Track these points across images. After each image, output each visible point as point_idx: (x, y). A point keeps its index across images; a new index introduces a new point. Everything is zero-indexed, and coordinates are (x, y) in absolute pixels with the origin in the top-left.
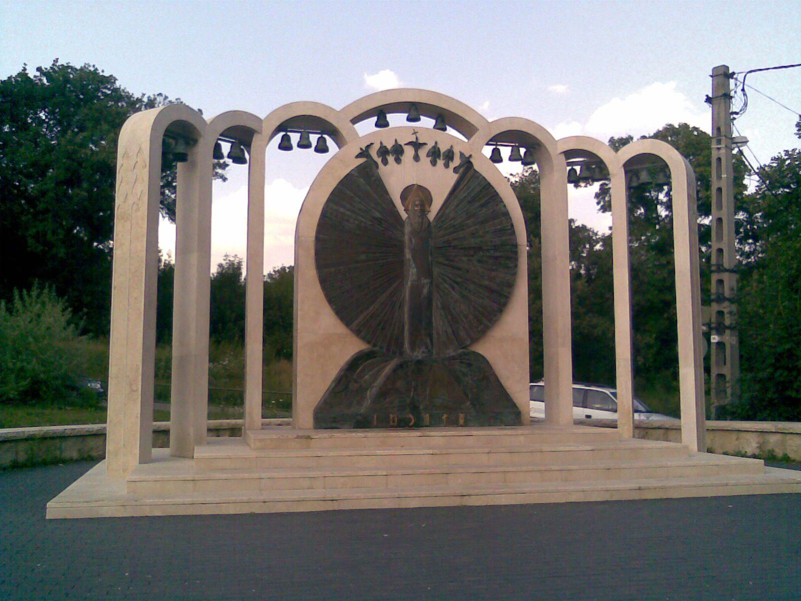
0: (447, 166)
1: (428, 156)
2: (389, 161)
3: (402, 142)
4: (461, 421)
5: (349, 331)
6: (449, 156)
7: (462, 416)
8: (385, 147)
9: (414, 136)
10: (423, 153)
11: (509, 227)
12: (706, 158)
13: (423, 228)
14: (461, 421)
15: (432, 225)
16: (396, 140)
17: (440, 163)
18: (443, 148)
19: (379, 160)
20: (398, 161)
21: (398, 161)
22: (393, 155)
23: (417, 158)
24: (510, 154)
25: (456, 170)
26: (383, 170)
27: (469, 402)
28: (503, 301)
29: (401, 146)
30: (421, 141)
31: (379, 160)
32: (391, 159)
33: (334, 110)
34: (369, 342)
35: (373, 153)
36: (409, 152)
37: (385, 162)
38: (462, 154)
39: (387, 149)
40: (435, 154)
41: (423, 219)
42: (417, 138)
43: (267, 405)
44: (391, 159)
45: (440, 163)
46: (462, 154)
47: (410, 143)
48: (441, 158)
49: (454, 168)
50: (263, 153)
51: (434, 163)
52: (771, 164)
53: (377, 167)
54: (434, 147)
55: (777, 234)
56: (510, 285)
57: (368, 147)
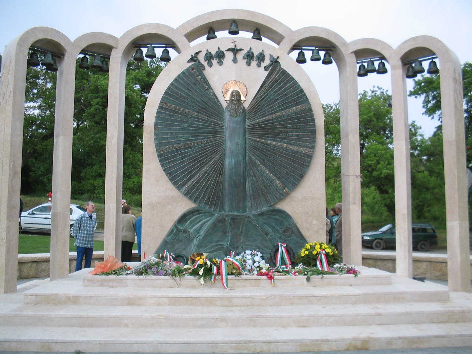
0: (259, 65)
1: (244, 58)
2: (213, 63)
3: (223, 49)
6: (261, 58)
8: (210, 53)
10: (240, 56)
15: (247, 111)
19: (205, 64)
20: (220, 63)
21: (220, 63)
22: (216, 59)
23: (235, 60)
24: (297, 56)
25: (266, 68)
30: (238, 48)
31: (205, 64)
32: (215, 62)
35: (201, 58)
36: (229, 56)
37: (210, 65)
40: (250, 57)
42: (235, 46)
44: (215, 62)
45: (254, 63)
47: (229, 50)
48: (255, 59)
49: (265, 67)
51: (249, 64)
54: (248, 52)
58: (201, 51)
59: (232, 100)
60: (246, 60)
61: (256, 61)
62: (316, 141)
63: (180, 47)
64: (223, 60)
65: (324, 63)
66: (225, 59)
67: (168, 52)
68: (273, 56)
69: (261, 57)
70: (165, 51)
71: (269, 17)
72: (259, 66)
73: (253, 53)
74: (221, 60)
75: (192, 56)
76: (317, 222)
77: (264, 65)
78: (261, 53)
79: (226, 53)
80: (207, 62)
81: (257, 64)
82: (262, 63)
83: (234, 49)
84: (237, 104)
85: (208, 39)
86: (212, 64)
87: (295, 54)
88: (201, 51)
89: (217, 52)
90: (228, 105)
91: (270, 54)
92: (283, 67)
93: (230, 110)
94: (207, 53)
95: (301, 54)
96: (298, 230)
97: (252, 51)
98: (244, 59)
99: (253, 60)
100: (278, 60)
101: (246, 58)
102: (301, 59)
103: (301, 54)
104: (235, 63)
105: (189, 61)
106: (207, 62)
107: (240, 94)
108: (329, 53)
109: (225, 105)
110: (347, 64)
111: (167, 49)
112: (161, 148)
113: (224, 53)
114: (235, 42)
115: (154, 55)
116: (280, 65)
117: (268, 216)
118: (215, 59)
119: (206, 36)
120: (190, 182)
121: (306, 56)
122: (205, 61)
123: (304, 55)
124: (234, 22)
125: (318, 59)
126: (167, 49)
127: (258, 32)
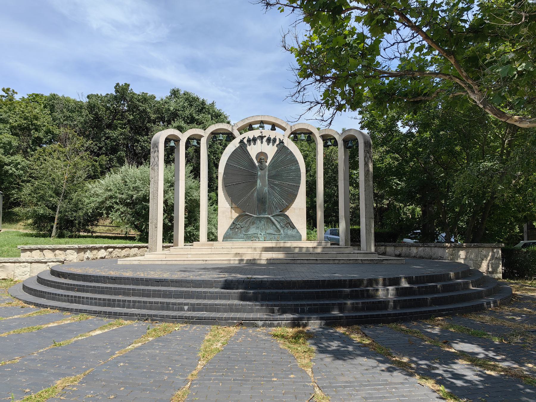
0: (273, 145)
12: (213, 118)
13: (35, 232)
20: (255, 144)
21: (255, 144)
23: (262, 143)
26: (249, 148)
30: (263, 135)
32: (252, 144)
37: (250, 145)
38: (280, 139)
40: (269, 140)
43: (423, 106)
44: (252, 144)
45: (271, 144)
51: (268, 144)
54: (268, 137)
55: (344, 104)
56: (298, 187)
57: (243, 139)
73: (271, 138)
77: (275, 144)
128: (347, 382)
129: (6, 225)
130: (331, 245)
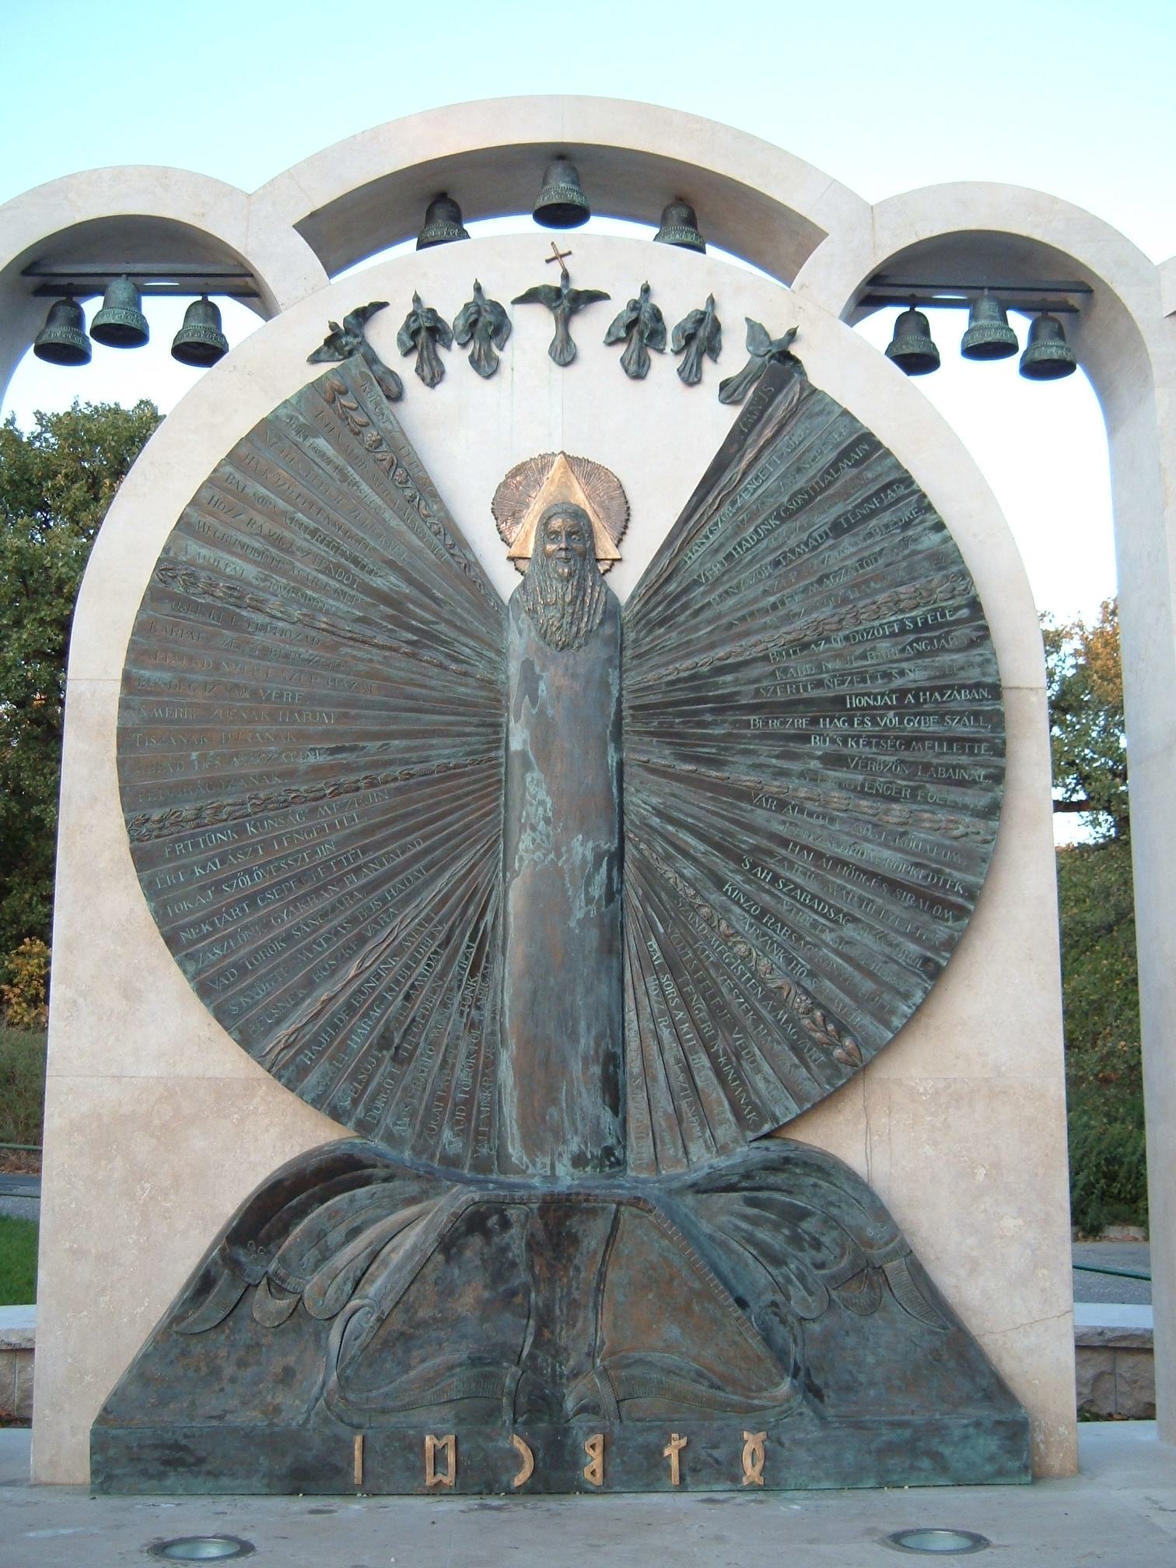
0: (691, 377)
1: (612, 341)
2: (448, 367)
3: (502, 293)
4: (751, 1471)
5: (260, 1072)
7: (752, 1443)
8: (432, 311)
9: (556, 269)
11: (964, 613)
14: (751, 1471)
15: (626, 615)
16: (478, 289)
17: (665, 365)
18: (675, 313)
19: (405, 368)
20: (485, 366)
21: (485, 366)
22: (464, 345)
23: (564, 353)
24: (890, 338)
25: (729, 391)
27: (788, 1380)
28: (941, 931)
29: (496, 307)
30: (579, 285)
31: (405, 368)
32: (455, 359)
33: (232, 191)
34: (337, 1115)
37: (433, 375)
38: (756, 331)
39: (439, 320)
41: (581, 588)
42: (566, 276)
44: (455, 359)
45: (665, 365)
46: (756, 331)
47: (531, 297)
48: (670, 346)
49: (724, 385)
50: (737, 376)
51: (638, 370)
52: (428, 380)
53: (396, 395)
54: (635, 306)
57: (363, 315)
58: (384, 305)
59: (549, 556)
60: (620, 350)
61: (677, 353)
62: (1010, 774)
63: (270, 285)
64: (501, 349)
65: (1035, 369)
66: (508, 345)
67: (214, 314)
68: (767, 328)
69: (702, 333)
70: (201, 310)
71: (739, 135)
72: (693, 379)
73: (657, 315)
74: (490, 346)
75: (333, 326)
76: (1020, 1222)
77: (714, 373)
78: (704, 313)
79: (518, 316)
80: (413, 360)
81: (680, 372)
82: (707, 363)
83: (558, 292)
84: (571, 575)
85: (420, 246)
86: (442, 373)
87: (883, 322)
88: (384, 305)
89: (467, 306)
90: (523, 585)
91: (747, 319)
92: (816, 379)
93: (535, 611)
94: (413, 314)
95: (913, 327)
96: (917, 1271)
97: (657, 300)
98: (611, 344)
99: (661, 351)
100: (795, 350)
101: (618, 341)
102: (913, 347)
103: (913, 327)
104: (566, 364)
105: (318, 352)
106: (414, 359)
107: (590, 524)
108: (1054, 320)
109: (506, 581)
110: (1157, 373)
111: (211, 299)
112: (156, 816)
113: (503, 313)
114: (566, 260)
115: (134, 324)
116: (803, 373)
117: (746, 1193)
118: (455, 344)
119: (415, 241)
120: (309, 1006)
121: (935, 336)
122: (407, 353)
123: (925, 329)
124: (562, 155)
125: (1001, 349)
126: (211, 299)
127: (684, 213)
128: (747, 634)
129: (1146, 1330)
130: (267, 600)
